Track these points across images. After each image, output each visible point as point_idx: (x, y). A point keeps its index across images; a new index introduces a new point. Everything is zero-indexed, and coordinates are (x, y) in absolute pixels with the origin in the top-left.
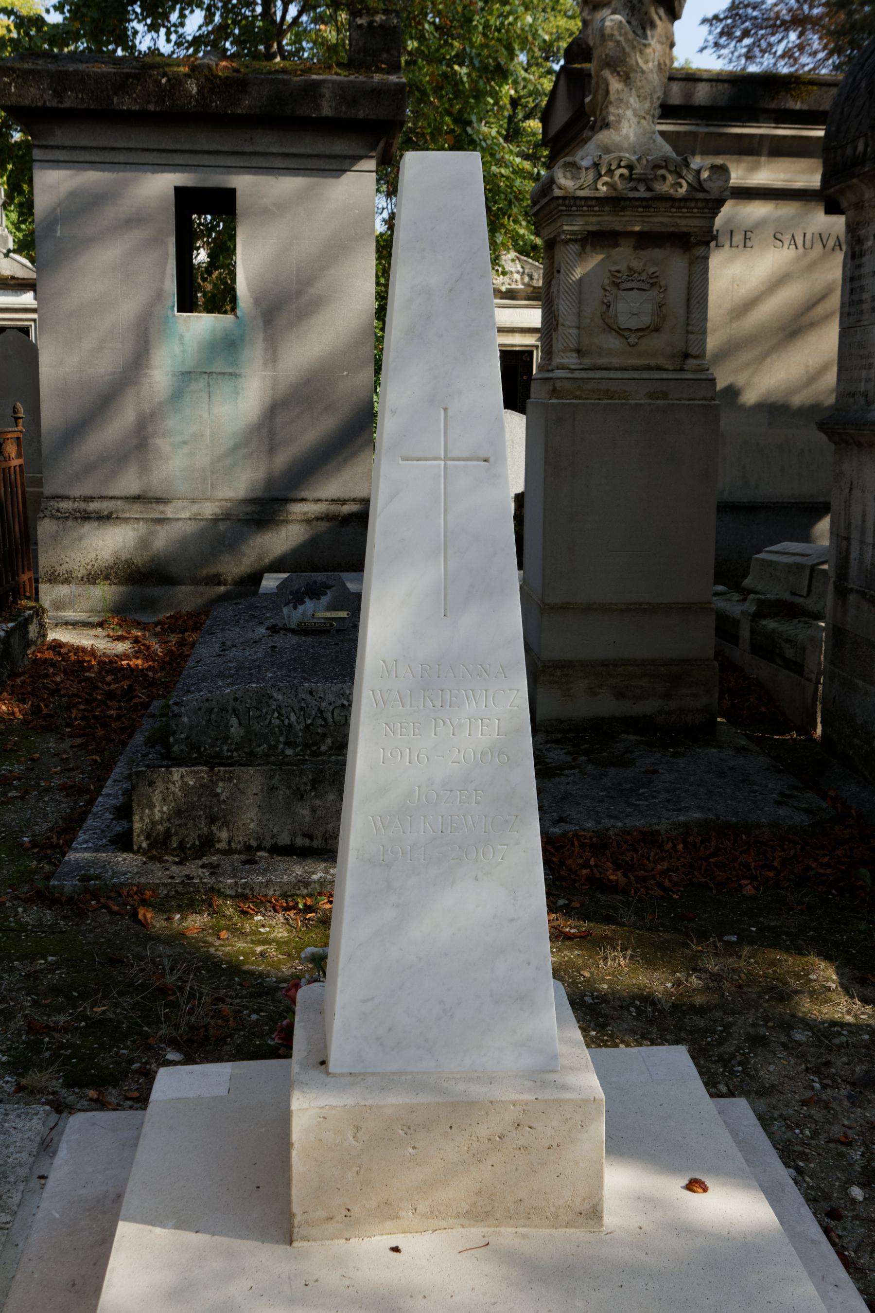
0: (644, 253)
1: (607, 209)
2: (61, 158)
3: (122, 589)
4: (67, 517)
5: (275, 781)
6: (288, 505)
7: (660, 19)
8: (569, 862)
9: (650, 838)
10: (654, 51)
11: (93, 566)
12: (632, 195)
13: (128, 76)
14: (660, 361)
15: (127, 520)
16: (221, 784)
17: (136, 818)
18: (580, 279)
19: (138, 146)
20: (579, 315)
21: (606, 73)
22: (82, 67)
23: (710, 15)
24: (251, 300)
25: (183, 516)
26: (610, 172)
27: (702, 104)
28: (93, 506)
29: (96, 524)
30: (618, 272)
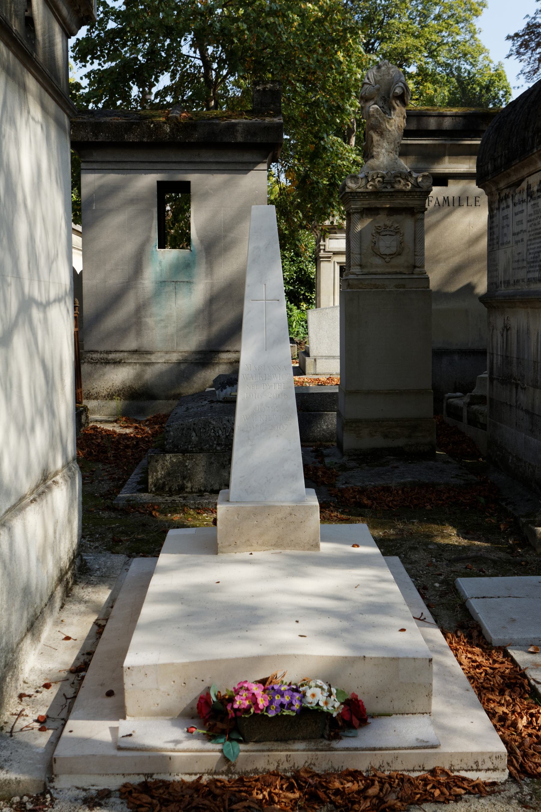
0: (392, 217)
1: (372, 197)
2: (96, 168)
3: (127, 402)
4: (97, 363)
5: (212, 460)
6: (219, 355)
7: (398, 106)
8: (346, 495)
9: (387, 489)
10: (395, 121)
11: (111, 389)
12: (384, 190)
13: (133, 123)
14: (402, 270)
15: (130, 364)
16: (188, 461)
17: (150, 477)
18: (361, 231)
19: (137, 160)
20: (361, 248)
21: (372, 133)
22: (108, 119)
23: (512, 34)
24: (199, 241)
25: (161, 361)
26: (373, 180)
27: (448, 129)
28: (111, 356)
29: (113, 366)
30: (379, 227)
